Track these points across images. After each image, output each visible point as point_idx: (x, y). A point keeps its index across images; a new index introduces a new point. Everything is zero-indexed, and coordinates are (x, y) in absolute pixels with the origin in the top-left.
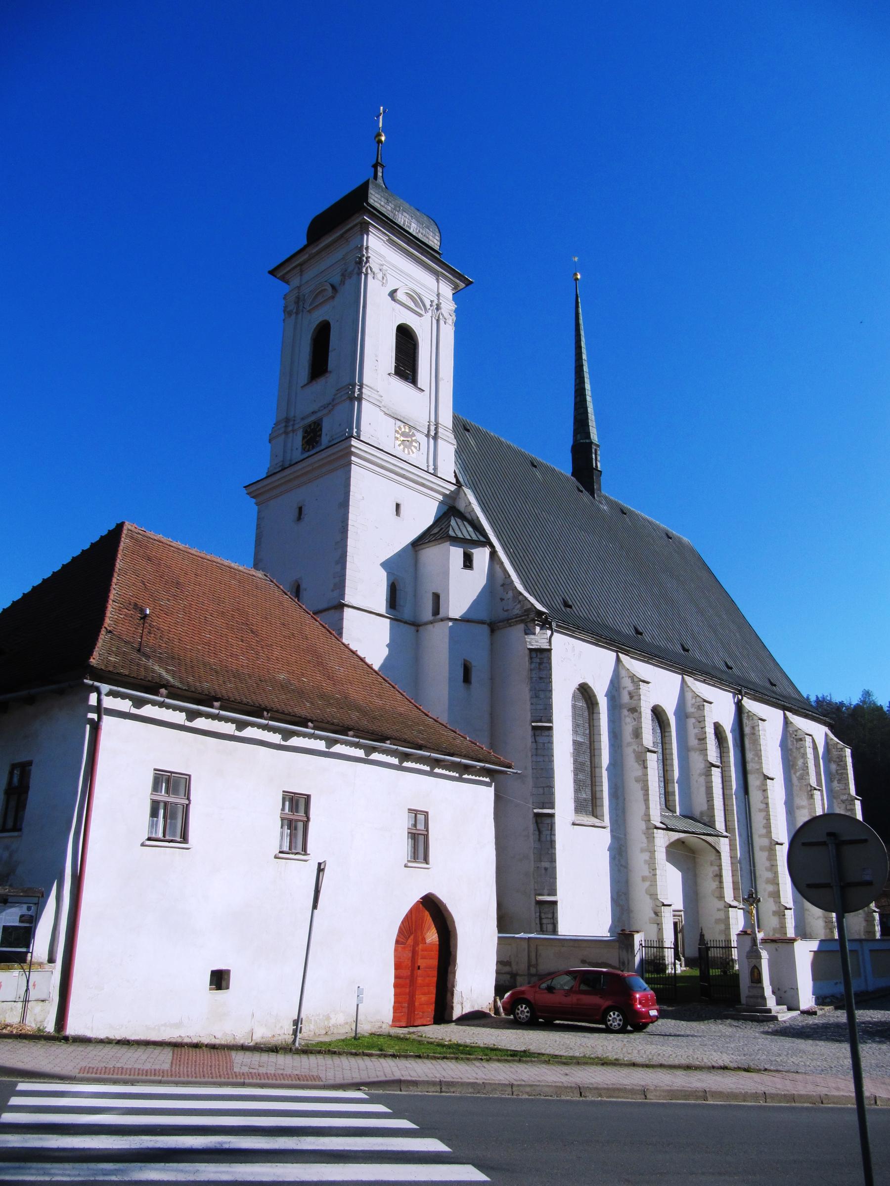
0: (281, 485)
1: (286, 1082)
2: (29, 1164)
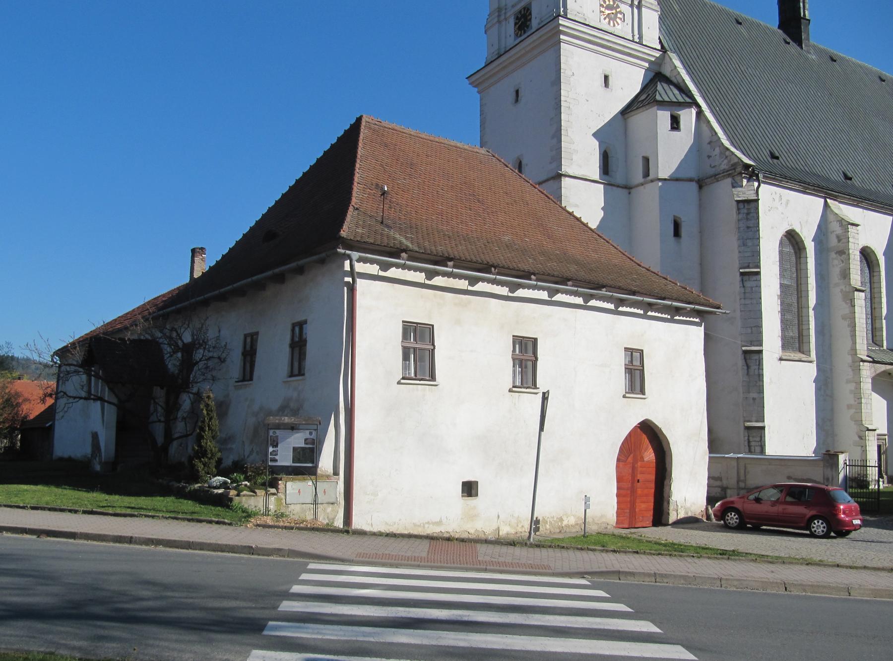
0: (498, 72)
1: (521, 569)
2: (307, 625)
